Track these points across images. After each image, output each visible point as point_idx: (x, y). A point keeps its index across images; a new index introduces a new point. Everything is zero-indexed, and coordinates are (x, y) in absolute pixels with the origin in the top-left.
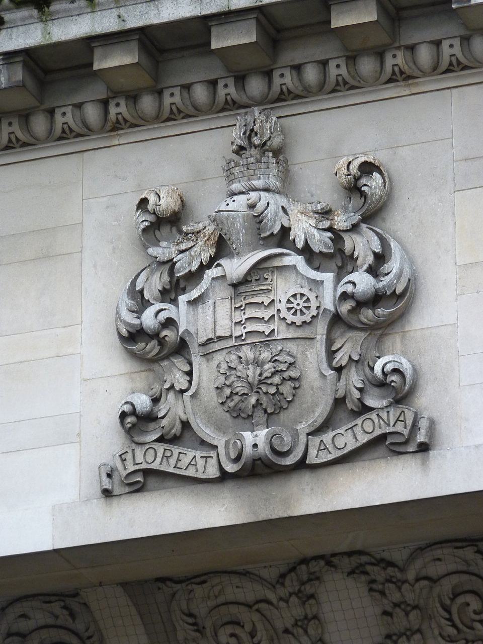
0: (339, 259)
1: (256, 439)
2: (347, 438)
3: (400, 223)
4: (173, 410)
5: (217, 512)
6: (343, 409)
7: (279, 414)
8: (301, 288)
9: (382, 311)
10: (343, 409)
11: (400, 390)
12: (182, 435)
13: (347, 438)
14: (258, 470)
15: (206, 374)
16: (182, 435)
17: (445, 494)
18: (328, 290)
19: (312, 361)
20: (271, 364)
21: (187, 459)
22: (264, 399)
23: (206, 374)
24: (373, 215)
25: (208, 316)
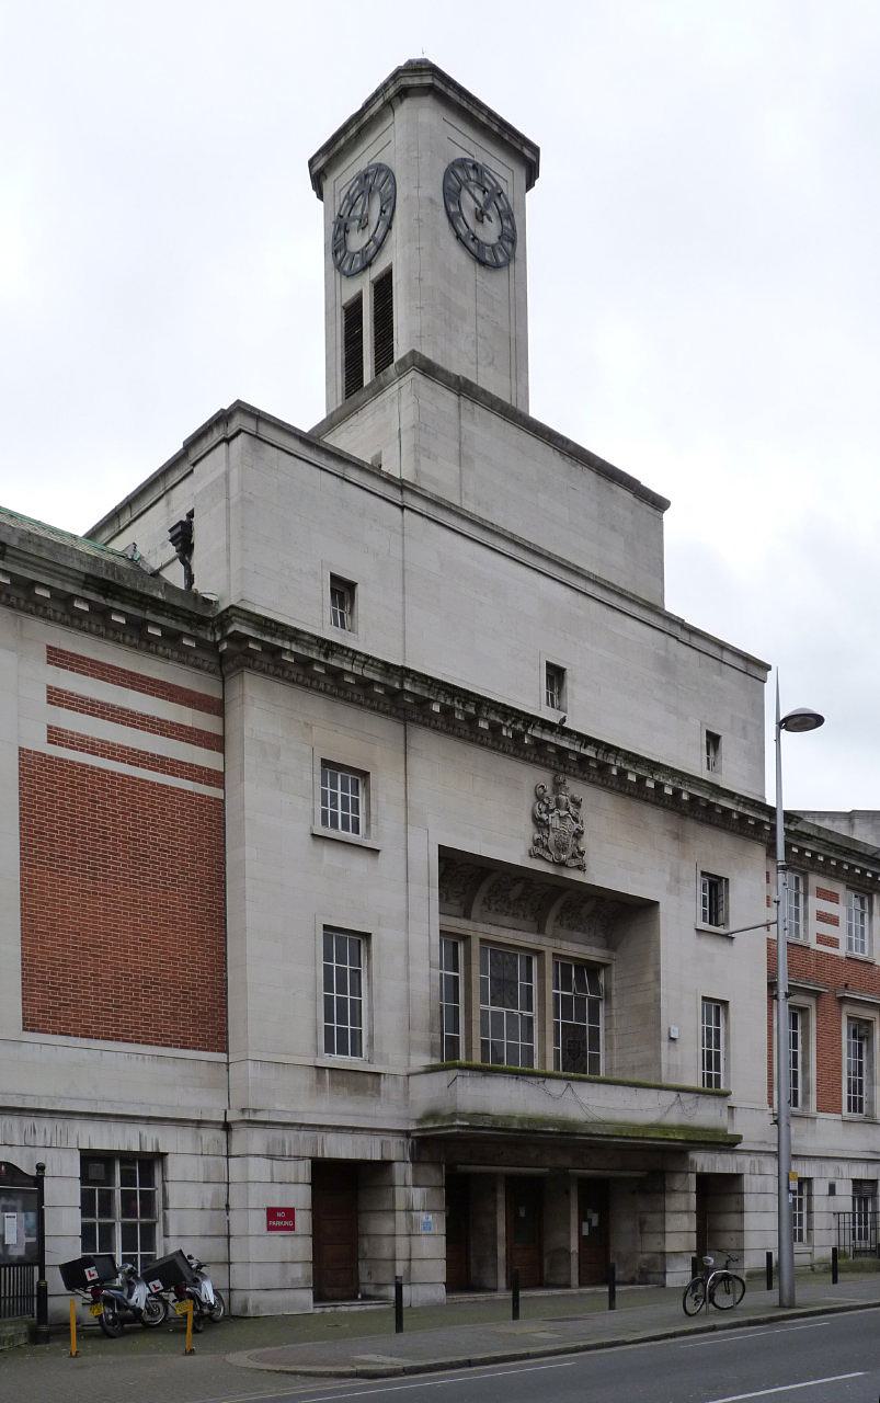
5: (550, 870)
9: (578, 835)
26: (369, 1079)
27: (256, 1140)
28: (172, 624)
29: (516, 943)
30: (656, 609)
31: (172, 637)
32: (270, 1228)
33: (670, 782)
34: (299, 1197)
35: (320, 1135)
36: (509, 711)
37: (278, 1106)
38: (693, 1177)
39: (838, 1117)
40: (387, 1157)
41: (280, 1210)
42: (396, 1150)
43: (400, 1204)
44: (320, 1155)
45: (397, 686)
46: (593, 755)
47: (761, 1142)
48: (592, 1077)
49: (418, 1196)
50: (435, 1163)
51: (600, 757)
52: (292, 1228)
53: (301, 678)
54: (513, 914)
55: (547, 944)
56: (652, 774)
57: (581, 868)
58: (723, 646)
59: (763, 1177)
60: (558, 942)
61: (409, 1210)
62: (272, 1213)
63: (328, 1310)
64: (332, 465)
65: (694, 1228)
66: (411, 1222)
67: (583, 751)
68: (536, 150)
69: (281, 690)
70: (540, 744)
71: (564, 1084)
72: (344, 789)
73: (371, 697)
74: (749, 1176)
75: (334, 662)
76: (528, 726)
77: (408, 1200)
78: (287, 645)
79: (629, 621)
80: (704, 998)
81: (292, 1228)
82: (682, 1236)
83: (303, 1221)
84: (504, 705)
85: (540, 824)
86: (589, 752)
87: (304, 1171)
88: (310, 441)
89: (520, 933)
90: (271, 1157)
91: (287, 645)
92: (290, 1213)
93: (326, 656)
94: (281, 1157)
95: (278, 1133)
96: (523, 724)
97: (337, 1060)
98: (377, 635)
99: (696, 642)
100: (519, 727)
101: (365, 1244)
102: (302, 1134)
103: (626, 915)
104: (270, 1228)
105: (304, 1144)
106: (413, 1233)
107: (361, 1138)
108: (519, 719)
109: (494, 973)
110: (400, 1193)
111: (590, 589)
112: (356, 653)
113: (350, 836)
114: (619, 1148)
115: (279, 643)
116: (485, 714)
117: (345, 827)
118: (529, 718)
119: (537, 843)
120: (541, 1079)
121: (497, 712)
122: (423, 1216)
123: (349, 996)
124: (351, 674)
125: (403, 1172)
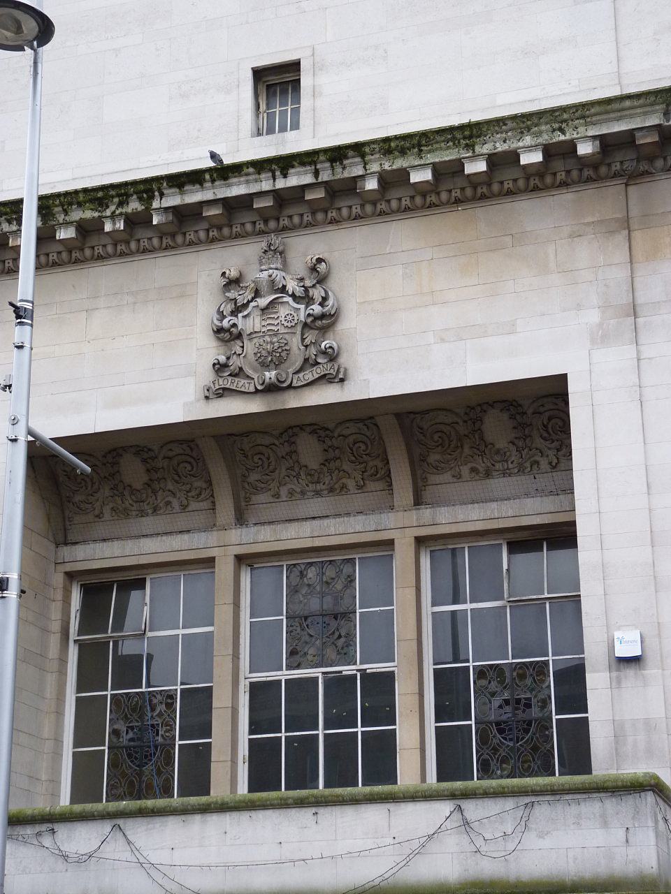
0: (307, 299)
1: (270, 375)
2: (309, 376)
4: (235, 362)
5: (254, 406)
6: (308, 363)
8: (290, 312)
9: (325, 322)
10: (308, 363)
11: (332, 356)
12: (239, 373)
13: (309, 376)
14: (271, 389)
15: (250, 347)
16: (239, 373)
18: (302, 312)
19: (295, 342)
21: (241, 384)
22: (276, 358)
23: (250, 347)
24: (322, 280)
25: (251, 323)
29: (318, 543)
33: (528, 140)
36: (100, 194)
46: (308, 179)
48: (193, 800)
51: (325, 176)
53: (575, 174)
54: (331, 490)
55: (401, 524)
56: (470, 147)
57: (337, 378)
60: (426, 513)
67: (281, 184)
70: (184, 216)
71: (106, 827)
76: (152, 197)
84: (85, 190)
85: (226, 335)
86: (299, 178)
89: (326, 522)
96: (140, 199)
100: (134, 206)
103: (532, 419)
108: (128, 195)
109: (354, 590)
116: (61, 218)
118: (142, 187)
119: (219, 368)
120: (44, 827)
121: (80, 205)
123: (109, 693)
124: (261, 194)
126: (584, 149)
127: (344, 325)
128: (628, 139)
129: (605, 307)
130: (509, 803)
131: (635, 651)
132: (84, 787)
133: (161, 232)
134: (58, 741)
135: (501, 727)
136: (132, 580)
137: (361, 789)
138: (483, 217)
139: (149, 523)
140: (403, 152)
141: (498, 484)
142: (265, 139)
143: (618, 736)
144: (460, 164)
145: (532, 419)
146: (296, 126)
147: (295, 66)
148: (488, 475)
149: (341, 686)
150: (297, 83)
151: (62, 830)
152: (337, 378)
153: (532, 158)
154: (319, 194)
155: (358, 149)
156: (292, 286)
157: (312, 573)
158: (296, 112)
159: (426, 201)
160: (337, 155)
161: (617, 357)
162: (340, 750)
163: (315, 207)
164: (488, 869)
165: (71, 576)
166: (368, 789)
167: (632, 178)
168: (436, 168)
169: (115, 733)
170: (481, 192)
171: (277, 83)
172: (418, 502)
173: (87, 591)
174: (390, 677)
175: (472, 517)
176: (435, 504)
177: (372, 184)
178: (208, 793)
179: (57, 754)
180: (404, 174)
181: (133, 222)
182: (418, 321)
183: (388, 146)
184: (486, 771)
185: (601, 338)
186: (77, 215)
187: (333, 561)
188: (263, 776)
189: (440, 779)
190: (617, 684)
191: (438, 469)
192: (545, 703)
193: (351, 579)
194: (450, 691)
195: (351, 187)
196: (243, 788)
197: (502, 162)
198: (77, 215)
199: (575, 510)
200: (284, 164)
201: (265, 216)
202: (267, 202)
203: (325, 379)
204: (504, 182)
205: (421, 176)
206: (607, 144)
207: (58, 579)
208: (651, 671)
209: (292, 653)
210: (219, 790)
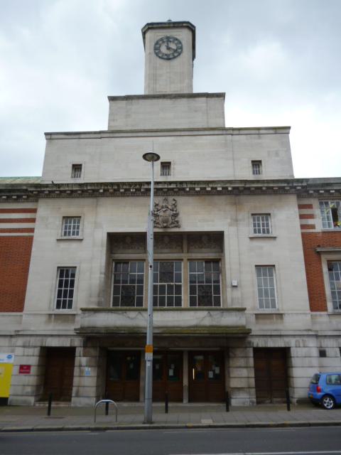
0: (173, 210)
1: (165, 225)
2: (173, 225)
3: (177, 208)
4: (157, 221)
5: (161, 230)
6: (172, 223)
7: (331, 393)
8: (169, 212)
9: (176, 215)
10: (172, 223)
11: (177, 222)
12: (158, 223)
13: (173, 225)
14: (165, 227)
15: (160, 219)
16: (158, 223)
17: (308, 302)
18: (172, 213)
19: (170, 218)
20: (21, 349)
21: (158, 225)
22: (166, 221)
23: (160, 219)
24: (176, 207)
25: (161, 213)
26: (70, 317)
27: (20, 341)
28: (19, 194)
30: (224, 129)
31: (9, 197)
32: (20, 372)
34: (33, 360)
35: (44, 338)
37: (32, 329)
38: (251, 350)
39: (325, 313)
40: (73, 345)
41: (25, 366)
42: (77, 342)
43: (77, 363)
44: (44, 345)
45: (85, 189)
47: (306, 330)
49: (84, 360)
50: (94, 347)
51: (178, 186)
52: (29, 373)
55: (185, 256)
57: (178, 226)
58: (259, 129)
59: (306, 349)
60: (190, 254)
61: (80, 366)
62: (22, 367)
63: (42, 405)
64: (77, 136)
65: (253, 375)
66: (81, 372)
67: (169, 187)
68: (195, 27)
69: (50, 201)
71: (137, 313)
72: (263, 220)
73: (175, 192)
74: (294, 348)
75: (61, 189)
77: (80, 362)
78: (45, 189)
79: (205, 137)
80: (256, 266)
81: (29, 373)
82: (243, 380)
83: (33, 370)
86: (172, 186)
87: (37, 351)
88: (112, 133)
90: (24, 347)
91: (45, 189)
92: (29, 367)
93: (59, 188)
94: (29, 347)
95: (28, 338)
97: (62, 311)
98: (88, 177)
99: (242, 132)
100: (138, 187)
101: (291, 379)
102: (38, 338)
103: (216, 239)
104: (20, 372)
105: (37, 342)
106: (86, 376)
107: (62, 339)
110: (77, 359)
111: (183, 133)
112: (68, 184)
113: (266, 235)
114: (197, 338)
115: (43, 189)
117: (264, 232)
122: (86, 369)
125: (79, 351)
126: (230, 189)
127: (180, 216)
128: (238, 188)
129: (231, 219)
130: (218, 312)
131: (236, 284)
132: (115, 304)
133: (142, 193)
134: (110, 293)
135: (203, 297)
136: (126, 262)
137: (166, 307)
138: (208, 198)
139: (130, 251)
140: (195, 184)
141: (204, 250)
142: (165, 177)
143: (232, 299)
144: (205, 188)
145: (216, 239)
146: (80, 177)
147: (170, 163)
148: (201, 248)
149: (170, 287)
150: (81, 169)
151: (128, 313)
152: (178, 226)
153: (219, 189)
154: (177, 190)
155: (186, 182)
156: (170, 207)
157: (165, 264)
158: (80, 174)
159: (198, 194)
160: (181, 183)
161: (233, 229)
162: (170, 299)
163: (175, 192)
164: (214, 323)
165: (113, 260)
166: (168, 307)
167: (237, 195)
168: (201, 188)
169: (122, 293)
170: (208, 193)
171: (77, 168)
172: (188, 252)
173: (116, 264)
174: (180, 286)
175: (199, 256)
176: (192, 252)
177: (188, 189)
178: (142, 306)
179: (110, 296)
180: (194, 188)
181: (126, 190)
182: (195, 218)
183: (191, 182)
184: (199, 305)
185: (230, 225)
186: (125, 187)
187: (170, 261)
188: (192, 302)
189: (113, 305)
190: (232, 291)
191: (192, 246)
192: (211, 292)
193: (173, 266)
194: (192, 290)
195: (184, 189)
196: (111, 306)
197: (225, 188)
198: (125, 187)
199: (154, 260)
200: (258, 181)
201: (165, 192)
202: (47, 192)
203: (176, 227)
204: (214, 192)
205: (197, 189)
206: (234, 188)
207: (111, 260)
208: (239, 288)
209: (160, 279)
210: (183, 306)
